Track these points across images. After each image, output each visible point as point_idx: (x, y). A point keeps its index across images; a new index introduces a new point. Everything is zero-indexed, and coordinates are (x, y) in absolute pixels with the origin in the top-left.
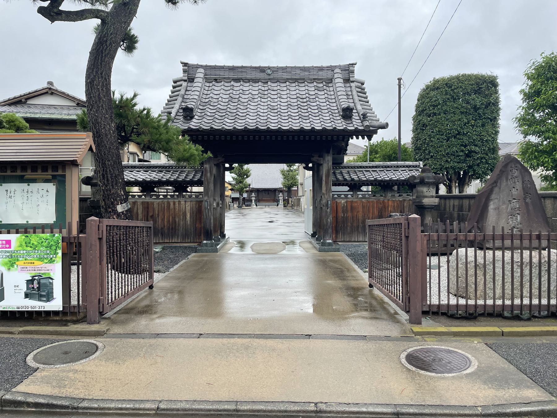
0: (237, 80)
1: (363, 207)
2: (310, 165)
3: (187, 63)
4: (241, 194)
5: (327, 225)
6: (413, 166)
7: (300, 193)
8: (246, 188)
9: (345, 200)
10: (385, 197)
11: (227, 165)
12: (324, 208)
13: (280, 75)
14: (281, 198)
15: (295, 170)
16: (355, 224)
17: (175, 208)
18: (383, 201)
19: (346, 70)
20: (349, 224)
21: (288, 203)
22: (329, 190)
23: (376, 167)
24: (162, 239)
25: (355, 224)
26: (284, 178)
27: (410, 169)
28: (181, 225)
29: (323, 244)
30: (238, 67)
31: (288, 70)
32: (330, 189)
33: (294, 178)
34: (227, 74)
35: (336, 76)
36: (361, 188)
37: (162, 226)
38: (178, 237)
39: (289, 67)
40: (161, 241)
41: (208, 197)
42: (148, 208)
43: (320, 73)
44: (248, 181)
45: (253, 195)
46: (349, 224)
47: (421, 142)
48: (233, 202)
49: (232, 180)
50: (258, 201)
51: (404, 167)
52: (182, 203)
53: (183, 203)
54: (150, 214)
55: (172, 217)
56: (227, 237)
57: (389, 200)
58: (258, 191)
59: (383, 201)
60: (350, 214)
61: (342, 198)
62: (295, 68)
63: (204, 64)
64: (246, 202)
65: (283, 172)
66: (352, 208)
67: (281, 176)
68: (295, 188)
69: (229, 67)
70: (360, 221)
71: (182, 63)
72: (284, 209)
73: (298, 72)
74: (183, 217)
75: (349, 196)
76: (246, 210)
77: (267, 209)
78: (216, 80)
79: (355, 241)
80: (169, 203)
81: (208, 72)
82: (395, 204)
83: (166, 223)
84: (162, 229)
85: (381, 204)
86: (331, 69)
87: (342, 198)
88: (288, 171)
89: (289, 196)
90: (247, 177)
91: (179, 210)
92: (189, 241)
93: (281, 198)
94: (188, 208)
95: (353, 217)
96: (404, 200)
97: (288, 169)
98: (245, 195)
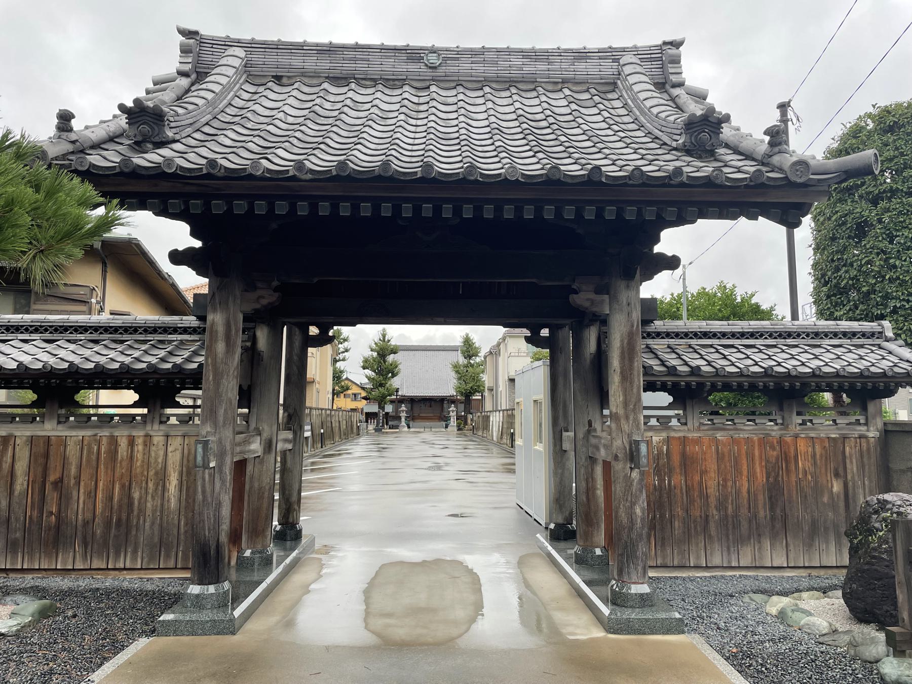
0: (340, 80)
1: (720, 457)
2: (545, 332)
3: (196, 33)
4: (382, 407)
5: (631, 529)
6: (864, 335)
7: (488, 406)
8: (390, 395)
9: (664, 435)
10: (785, 425)
11: (314, 330)
12: (618, 466)
13: (465, 67)
14: (453, 415)
15: (479, 365)
16: (696, 513)
17: (131, 458)
18: (781, 441)
19: (656, 59)
20: (679, 511)
21: (466, 423)
22: (632, 405)
23: (752, 335)
24: (84, 557)
25: (696, 513)
26: (459, 379)
27: (856, 341)
28: (149, 512)
29: (617, 600)
30: (344, 47)
31: (489, 56)
32: (639, 399)
33: (476, 378)
34: (311, 63)
35: (627, 70)
36: (79, 397)
37: (89, 516)
38: (135, 552)
39: (489, 50)
40: (79, 565)
41: (215, 424)
42: (47, 456)
43: (581, 66)
44: (395, 382)
45: (403, 407)
46: (679, 511)
47: (853, 273)
48: (367, 422)
49: (367, 381)
50: (412, 418)
51: (835, 335)
52: (156, 440)
53: (158, 439)
54: (52, 477)
55: (123, 486)
56: (304, 540)
57: (796, 436)
58: (412, 401)
59: (781, 441)
60: (678, 479)
61: (652, 428)
62: (509, 51)
63: (247, 36)
64: (391, 421)
65: (456, 367)
66: (687, 462)
67: (453, 374)
68: (477, 397)
69: (317, 45)
70: (713, 501)
71: (182, 32)
72: (459, 435)
73: (517, 61)
74: (156, 485)
75: (674, 422)
76: (389, 438)
77: (427, 435)
78: (278, 79)
79: (697, 567)
80: (113, 441)
81: (257, 58)
82: (818, 448)
83: (99, 510)
84: (86, 523)
85: (773, 448)
86: (612, 54)
87: (652, 428)
88: (466, 366)
89: (468, 410)
90: (394, 375)
91: (147, 464)
92: (171, 564)
93: (453, 415)
94: (174, 458)
95: (688, 489)
96: (844, 438)
97: (466, 362)
98: (389, 408)
